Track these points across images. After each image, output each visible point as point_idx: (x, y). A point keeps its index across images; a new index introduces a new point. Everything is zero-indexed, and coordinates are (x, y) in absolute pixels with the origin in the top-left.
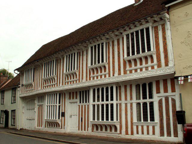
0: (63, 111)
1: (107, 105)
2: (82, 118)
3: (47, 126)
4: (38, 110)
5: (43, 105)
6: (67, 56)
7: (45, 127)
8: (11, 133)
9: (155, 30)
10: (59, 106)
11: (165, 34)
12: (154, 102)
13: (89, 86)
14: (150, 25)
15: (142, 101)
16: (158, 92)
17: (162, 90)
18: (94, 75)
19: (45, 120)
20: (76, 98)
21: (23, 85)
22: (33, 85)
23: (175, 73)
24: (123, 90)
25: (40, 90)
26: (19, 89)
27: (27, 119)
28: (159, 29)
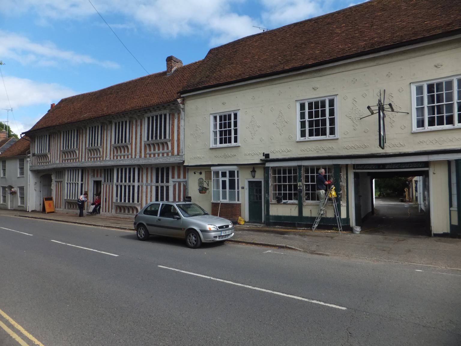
0: (86, 190)
1: (162, 187)
2: (106, 199)
3: (67, 208)
4: (56, 188)
5: (62, 181)
6: (90, 128)
7: (65, 208)
8: (20, 216)
9: (172, 117)
10: (82, 184)
11: (179, 123)
12: (169, 186)
13: (113, 166)
14: (167, 112)
15: (160, 184)
16: (173, 178)
17: (176, 176)
18: (159, 152)
19: (65, 200)
20: (101, 176)
21: (34, 155)
22: (49, 156)
23: (184, 162)
24: (145, 171)
25: (59, 164)
26: (28, 159)
27: (295, 210)
28: (175, 118)
